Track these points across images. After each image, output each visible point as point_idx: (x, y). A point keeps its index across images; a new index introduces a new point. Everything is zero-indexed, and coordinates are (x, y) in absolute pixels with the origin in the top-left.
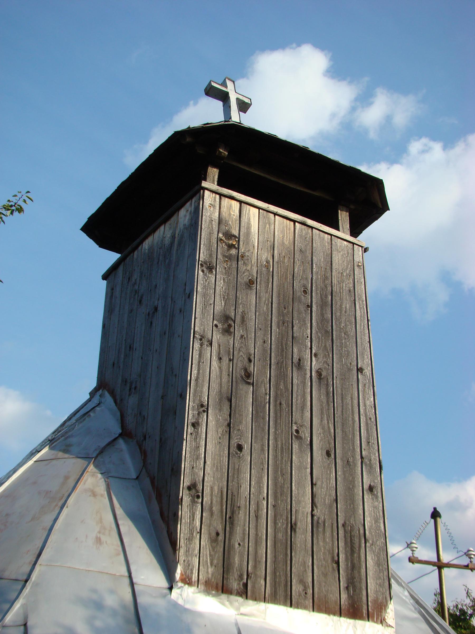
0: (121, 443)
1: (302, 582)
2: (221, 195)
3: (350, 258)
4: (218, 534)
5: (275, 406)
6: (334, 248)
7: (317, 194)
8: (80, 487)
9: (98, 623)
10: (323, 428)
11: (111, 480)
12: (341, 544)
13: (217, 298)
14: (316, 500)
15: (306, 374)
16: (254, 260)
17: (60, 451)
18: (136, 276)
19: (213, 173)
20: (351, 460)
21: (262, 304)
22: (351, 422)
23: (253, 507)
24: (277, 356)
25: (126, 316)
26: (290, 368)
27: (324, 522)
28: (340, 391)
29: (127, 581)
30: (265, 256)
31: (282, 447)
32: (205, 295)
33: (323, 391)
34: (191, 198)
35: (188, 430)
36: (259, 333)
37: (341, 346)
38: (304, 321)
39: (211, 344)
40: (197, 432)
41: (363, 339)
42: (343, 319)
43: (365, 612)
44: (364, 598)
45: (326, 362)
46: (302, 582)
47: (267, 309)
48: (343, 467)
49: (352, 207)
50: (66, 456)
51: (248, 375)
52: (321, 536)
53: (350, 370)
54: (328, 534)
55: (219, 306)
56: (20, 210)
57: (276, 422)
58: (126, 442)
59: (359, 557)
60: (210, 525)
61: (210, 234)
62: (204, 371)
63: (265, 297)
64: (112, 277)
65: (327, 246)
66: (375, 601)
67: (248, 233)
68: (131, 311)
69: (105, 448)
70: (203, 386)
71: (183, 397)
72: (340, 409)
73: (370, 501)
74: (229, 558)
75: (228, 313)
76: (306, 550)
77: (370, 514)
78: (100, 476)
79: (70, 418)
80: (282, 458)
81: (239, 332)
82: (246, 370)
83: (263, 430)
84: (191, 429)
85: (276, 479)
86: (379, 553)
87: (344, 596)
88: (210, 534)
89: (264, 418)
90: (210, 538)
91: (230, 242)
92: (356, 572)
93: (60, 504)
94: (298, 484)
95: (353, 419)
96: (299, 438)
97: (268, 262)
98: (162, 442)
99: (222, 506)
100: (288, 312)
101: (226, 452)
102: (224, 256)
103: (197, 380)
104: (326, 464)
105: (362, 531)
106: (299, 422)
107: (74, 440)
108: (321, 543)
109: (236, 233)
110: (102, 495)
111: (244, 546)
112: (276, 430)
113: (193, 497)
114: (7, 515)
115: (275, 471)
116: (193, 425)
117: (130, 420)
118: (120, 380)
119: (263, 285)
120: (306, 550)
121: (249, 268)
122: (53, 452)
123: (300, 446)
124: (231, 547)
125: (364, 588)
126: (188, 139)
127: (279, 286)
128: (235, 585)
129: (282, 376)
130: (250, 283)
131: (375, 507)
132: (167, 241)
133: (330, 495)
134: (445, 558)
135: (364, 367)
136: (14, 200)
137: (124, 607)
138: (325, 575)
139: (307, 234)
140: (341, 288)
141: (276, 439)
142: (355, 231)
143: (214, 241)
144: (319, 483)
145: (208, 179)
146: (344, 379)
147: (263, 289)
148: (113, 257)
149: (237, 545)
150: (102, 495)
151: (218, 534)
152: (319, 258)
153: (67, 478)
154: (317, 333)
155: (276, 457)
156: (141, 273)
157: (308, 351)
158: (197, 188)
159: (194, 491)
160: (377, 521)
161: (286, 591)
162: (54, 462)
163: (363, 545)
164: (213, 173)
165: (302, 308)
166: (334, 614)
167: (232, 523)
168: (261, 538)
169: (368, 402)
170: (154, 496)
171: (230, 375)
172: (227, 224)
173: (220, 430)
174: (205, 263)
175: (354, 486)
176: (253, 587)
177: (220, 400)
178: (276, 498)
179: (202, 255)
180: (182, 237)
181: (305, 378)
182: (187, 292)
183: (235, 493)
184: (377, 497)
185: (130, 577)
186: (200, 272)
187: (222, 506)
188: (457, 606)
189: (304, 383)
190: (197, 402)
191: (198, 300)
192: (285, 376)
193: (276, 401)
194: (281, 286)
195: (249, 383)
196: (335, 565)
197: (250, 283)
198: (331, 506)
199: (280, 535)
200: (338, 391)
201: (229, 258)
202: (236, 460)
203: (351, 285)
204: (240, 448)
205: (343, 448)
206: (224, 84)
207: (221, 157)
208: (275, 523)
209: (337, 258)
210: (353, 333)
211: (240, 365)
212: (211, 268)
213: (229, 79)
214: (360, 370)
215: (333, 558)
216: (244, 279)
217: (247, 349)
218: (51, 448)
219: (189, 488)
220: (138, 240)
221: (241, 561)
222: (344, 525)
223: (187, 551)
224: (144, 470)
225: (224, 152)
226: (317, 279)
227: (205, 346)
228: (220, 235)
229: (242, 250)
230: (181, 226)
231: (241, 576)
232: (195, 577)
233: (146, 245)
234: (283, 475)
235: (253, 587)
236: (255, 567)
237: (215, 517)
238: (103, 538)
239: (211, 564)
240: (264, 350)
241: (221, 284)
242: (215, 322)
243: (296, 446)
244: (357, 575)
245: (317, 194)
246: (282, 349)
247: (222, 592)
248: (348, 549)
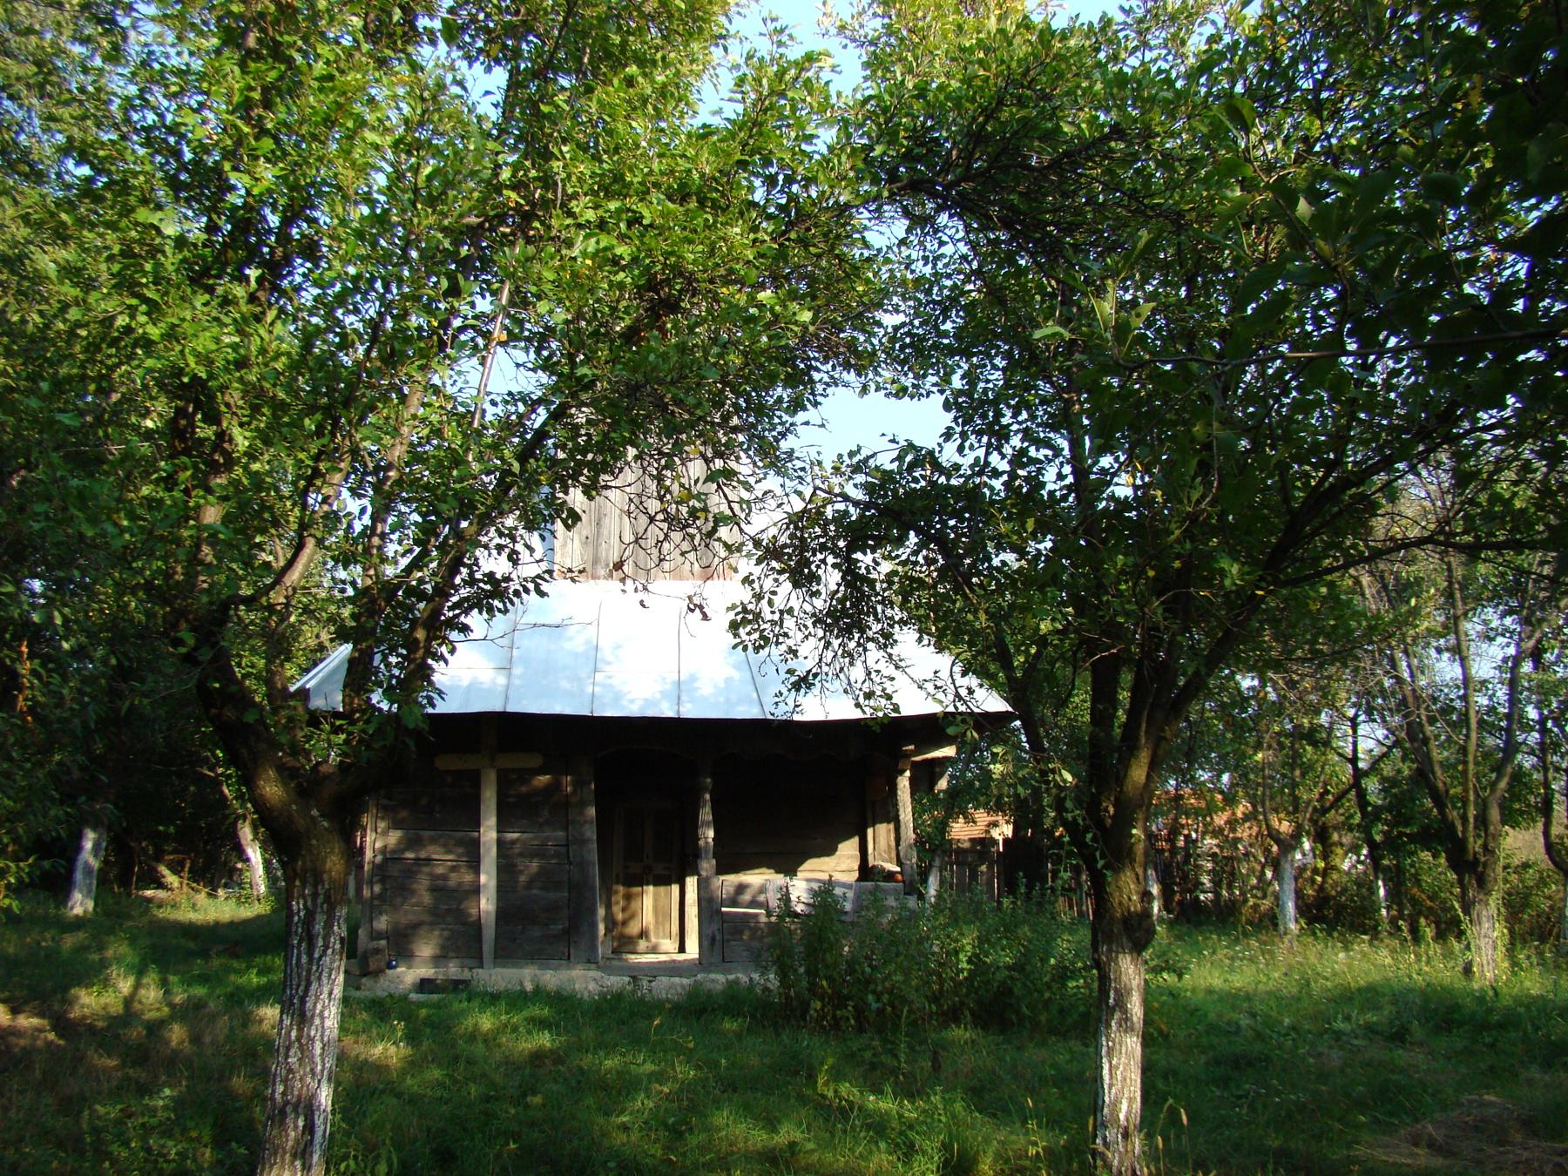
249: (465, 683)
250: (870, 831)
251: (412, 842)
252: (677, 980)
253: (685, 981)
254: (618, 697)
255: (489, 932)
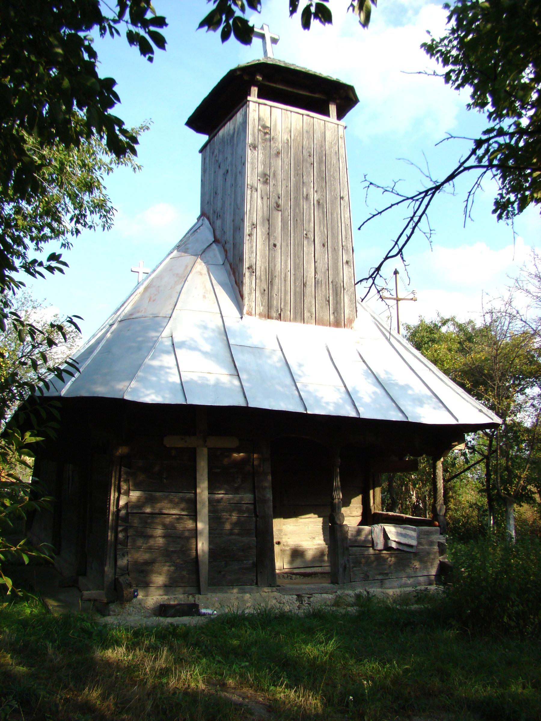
0: (214, 245)
1: (310, 311)
2: (259, 104)
3: (336, 133)
4: (264, 290)
5: (294, 221)
6: (326, 128)
7: (317, 96)
8: (194, 270)
9: (206, 335)
10: (321, 232)
11: (210, 266)
12: (331, 292)
13: (259, 164)
14: (317, 270)
15: (311, 203)
16: (280, 140)
17: (183, 252)
18: (216, 152)
19: (254, 90)
20: (336, 248)
21: (285, 165)
22: (336, 227)
23: (283, 276)
24: (294, 194)
25: (213, 175)
26: (302, 200)
27: (321, 281)
28: (330, 211)
29: (220, 315)
30: (286, 137)
31: (298, 244)
32: (252, 163)
33: (321, 211)
34: (243, 106)
35: (246, 238)
36: (284, 182)
37: (331, 186)
38: (309, 173)
39: (257, 191)
40: (251, 239)
41: (343, 180)
42: (332, 170)
43: (343, 324)
44: (343, 318)
45: (322, 195)
46: (310, 311)
47: (288, 167)
48: (332, 252)
49: (338, 101)
50: (186, 255)
51: (278, 206)
52: (320, 289)
53: (336, 198)
54: (323, 287)
55: (260, 169)
56: (148, 128)
57: (294, 230)
58: (217, 245)
59: (340, 297)
60: (260, 286)
61: (254, 127)
62: (254, 206)
63: (286, 160)
64: (204, 152)
65: (323, 128)
66: (349, 319)
67: (275, 125)
68: (215, 172)
69: (205, 249)
70: (253, 214)
71: (243, 220)
72: (330, 221)
73: (347, 269)
74: (271, 302)
75: (265, 172)
76: (312, 296)
77: (347, 276)
78: (203, 264)
79: (188, 233)
80: (298, 249)
81: (272, 182)
82: (277, 203)
83: (287, 235)
84: (248, 238)
85: (295, 260)
86: (351, 295)
87: (332, 317)
88: (260, 291)
89: (288, 229)
90: (260, 292)
91: (266, 131)
92: (338, 305)
93: (184, 280)
94: (307, 262)
95: (338, 226)
96: (307, 238)
97: (288, 140)
98: (234, 245)
99: (266, 276)
100: (300, 168)
101: (268, 248)
102: (262, 139)
103: (250, 211)
104: (322, 251)
105: (342, 285)
106: (307, 229)
107: (189, 246)
108: (320, 292)
109: (268, 125)
110: (205, 274)
111: (279, 295)
112: (294, 234)
113: (251, 273)
114: (159, 287)
115: (295, 257)
116: (249, 235)
117: (218, 233)
118: (212, 212)
119: (285, 154)
120: (312, 296)
121: (277, 145)
122: (179, 253)
123: (308, 242)
124: (272, 297)
125: (343, 312)
126: (238, 73)
127: (294, 154)
128: (274, 315)
129: (297, 204)
130: (278, 153)
131: (349, 272)
132: (231, 132)
133: (325, 267)
134: (400, 296)
135: (344, 196)
136: (144, 124)
137: (218, 328)
138: (322, 307)
139: (310, 121)
140: (331, 152)
141: (294, 240)
142: (340, 115)
143: (256, 131)
144: (319, 261)
145: (252, 95)
146: (333, 202)
147: (285, 156)
148: (204, 138)
149: (275, 295)
150: (205, 274)
151: (264, 290)
152: (318, 135)
153: (187, 266)
154: (317, 179)
155: (294, 249)
156: (219, 150)
157: (312, 189)
158: (245, 101)
159: (251, 269)
160: (350, 279)
161: (301, 316)
162: (180, 258)
163: (343, 292)
164: (254, 90)
165: (308, 165)
166: (327, 326)
167: (272, 285)
168: (288, 291)
169: (346, 216)
170: (232, 273)
171: (269, 207)
172: (263, 120)
173: (264, 237)
174: (252, 144)
175: (338, 262)
176: (284, 315)
177: (263, 221)
178: (295, 270)
179: (250, 140)
180: (239, 129)
181: (310, 205)
182: (243, 161)
183: (273, 269)
184: (350, 267)
185: (221, 313)
186: (249, 151)
187: (266, 276)
188: (432, 322)
189: (310, 208)
190: (251, 223)
191: (248, 166)
192: (299, 205)
193: (294, 219)
194: (296, 154)
195: (279, 210)
196: (327, 302)
197: (278, 153)
198: (325, 273)
199: (298, 289)
200: (329, 211)
201: (265, 140)
202: (273, 252)
203: (337, 149)
204: (275, 245)
205: (332, 241)
206: (262, 28)
207: (258, 81)
208: (295, 283)
209: (328, 134)
210: (338, 177)
211: (273, 201)
212: (255, 147)
213: (266, 25)
214: (342, 198)
215: (326, 299)
216: (273, 152)
217: (277, 191)
218: (178, 251)
219: (249, 268)
220: (216, 131)
221: (277, 303)
222: (332, 282)
223: (249, 300)
224: (405, 198)
225: (259, 78)
226: (316, 147)
227: (253, 192)
228: (260, 127)
229: (272, 134)
230: (238, 123)
231: (277, 310)
232: (253, 312)
233: (221, 133)
234: (299, 258)
235: (284, 315)
236: (285, 305)
237: (263, 282)
238: (206, 296)
239: (262, 306)
240: (287, 191)
241: (261, 156)
242: (259, 178)
243: (305, 242)
244: (339, 307)
245: (317, 96)
246: (297, 189)
247: (268, 318)
248: (335, 294)
249: (212, 382)
250: (371, 492)
251: (150, 500)
252: (325, 596)
253: (330, 596)
254: (318, 401)
255: (204, 569)
